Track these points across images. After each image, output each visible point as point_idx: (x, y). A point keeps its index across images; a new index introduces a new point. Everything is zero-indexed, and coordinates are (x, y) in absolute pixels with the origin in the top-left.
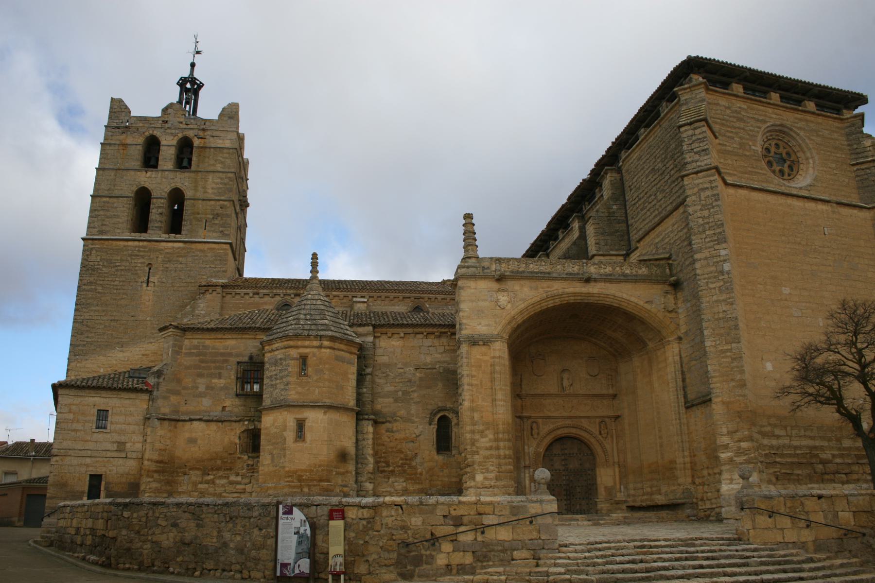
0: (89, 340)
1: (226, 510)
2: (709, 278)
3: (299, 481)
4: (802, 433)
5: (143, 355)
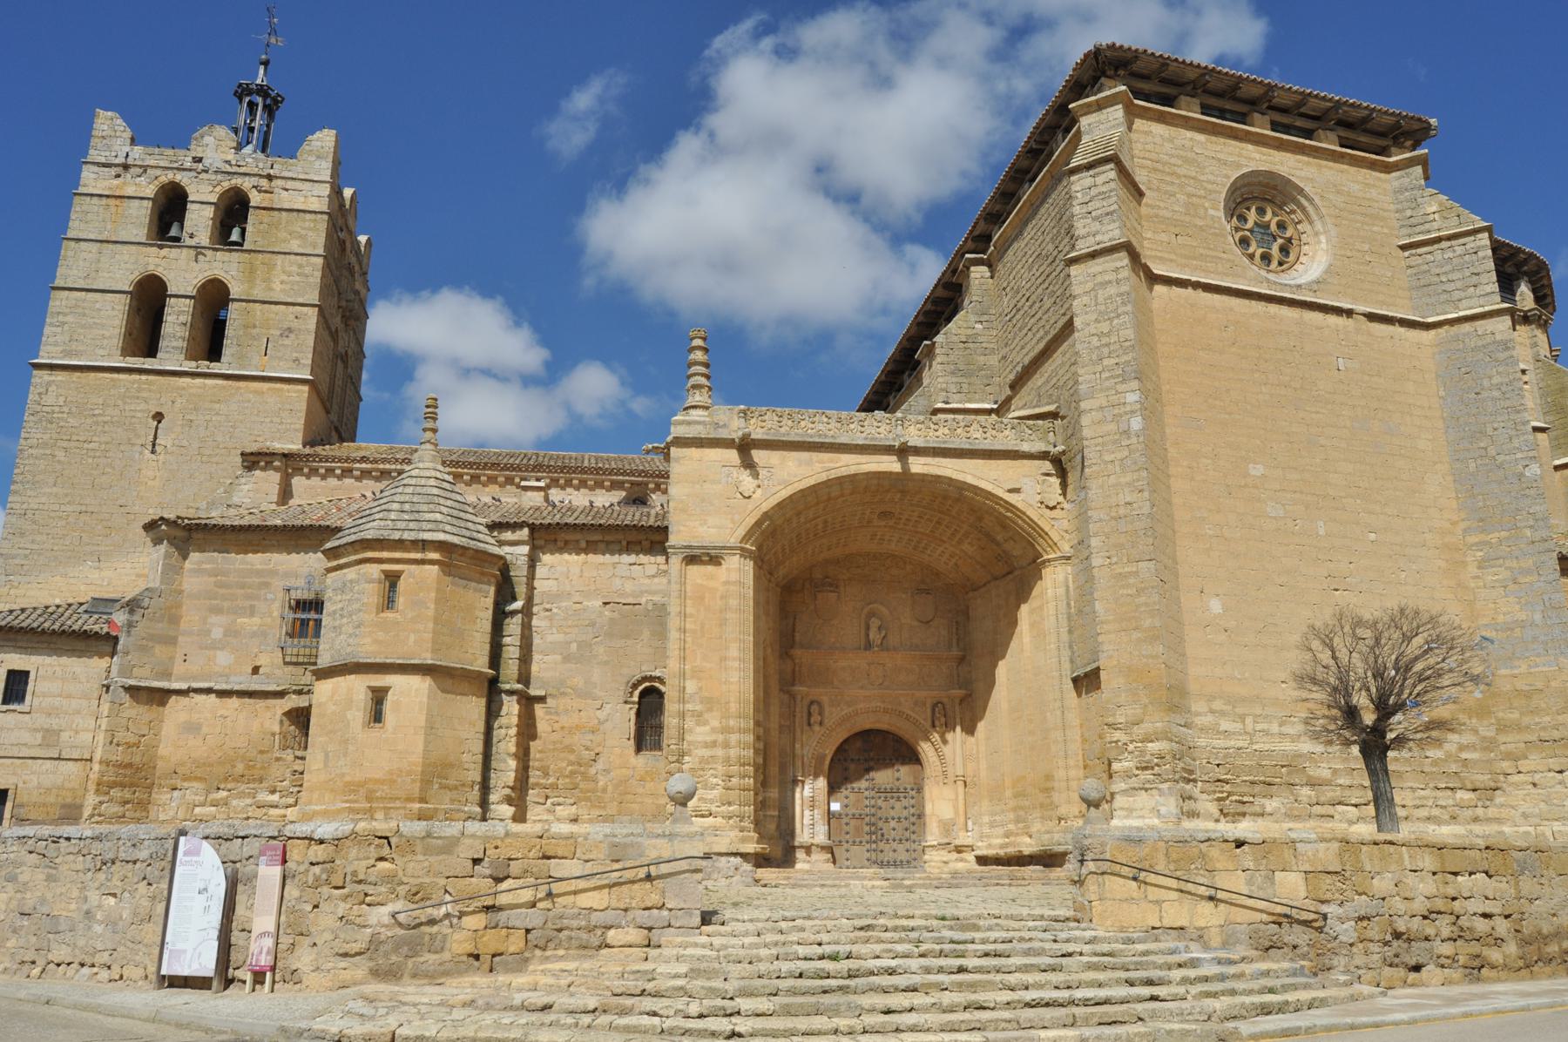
0: (35, 547)
1: (97, 847)
2: (1103, 444)
3: (369, 799)
4: (1275, 728)
5: (138, 576)
